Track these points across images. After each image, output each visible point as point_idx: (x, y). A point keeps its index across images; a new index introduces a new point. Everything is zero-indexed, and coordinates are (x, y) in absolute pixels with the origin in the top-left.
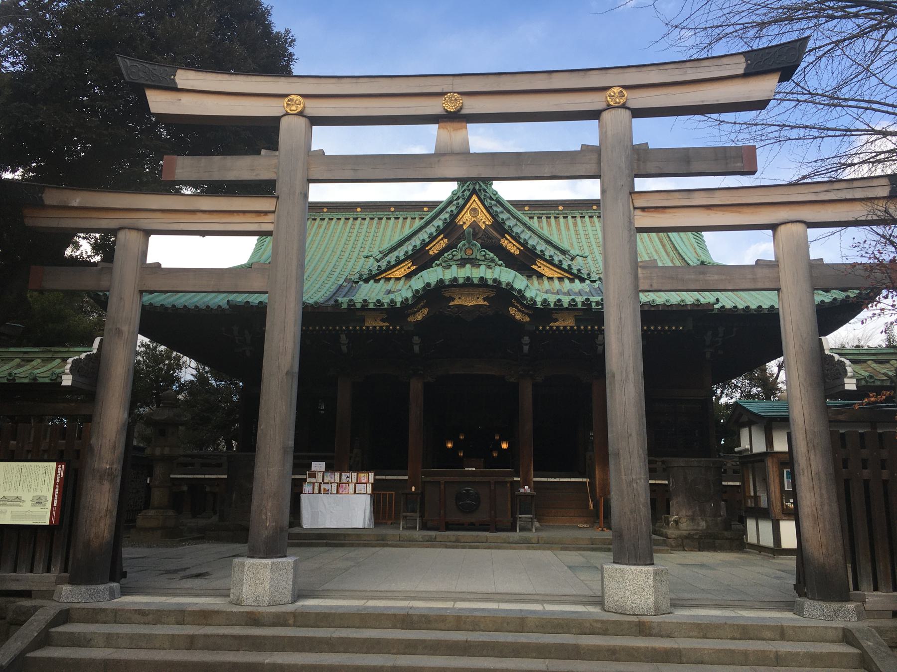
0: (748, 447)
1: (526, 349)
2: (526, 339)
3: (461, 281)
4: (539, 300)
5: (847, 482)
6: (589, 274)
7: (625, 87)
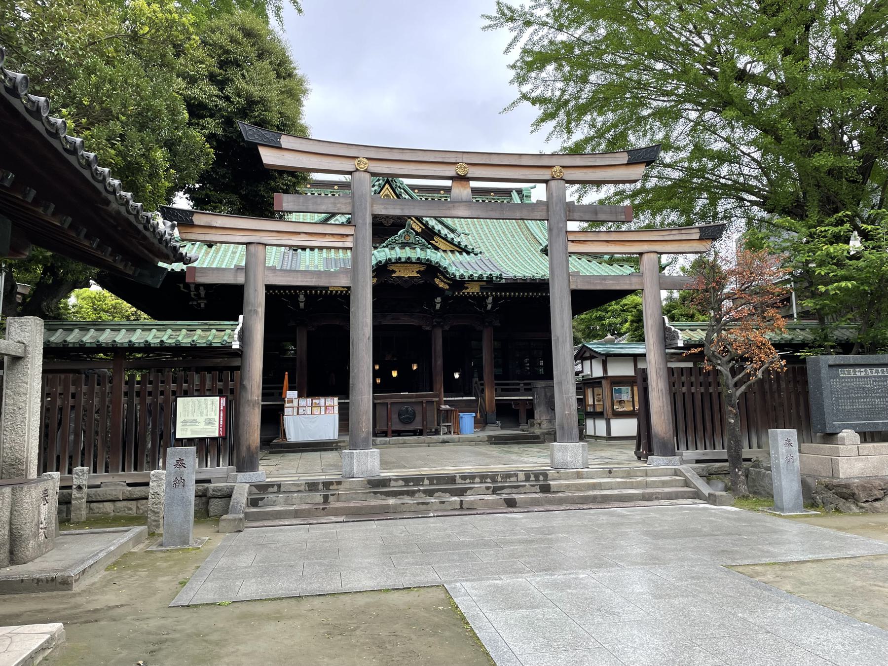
0: (589, 373)
1: (438, 306)
2: (439, 300)
3: (403, 260)
4: (457, 274)
5: (674, 394)
6: (473, 249)
7: (562, 167)
